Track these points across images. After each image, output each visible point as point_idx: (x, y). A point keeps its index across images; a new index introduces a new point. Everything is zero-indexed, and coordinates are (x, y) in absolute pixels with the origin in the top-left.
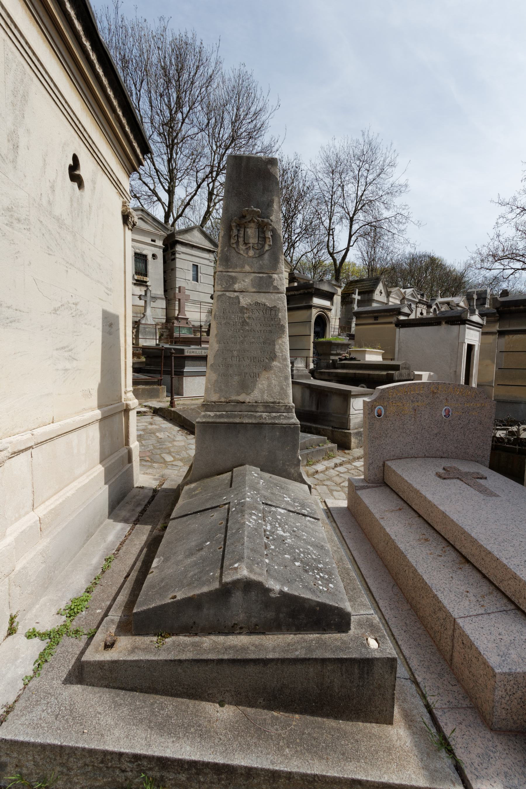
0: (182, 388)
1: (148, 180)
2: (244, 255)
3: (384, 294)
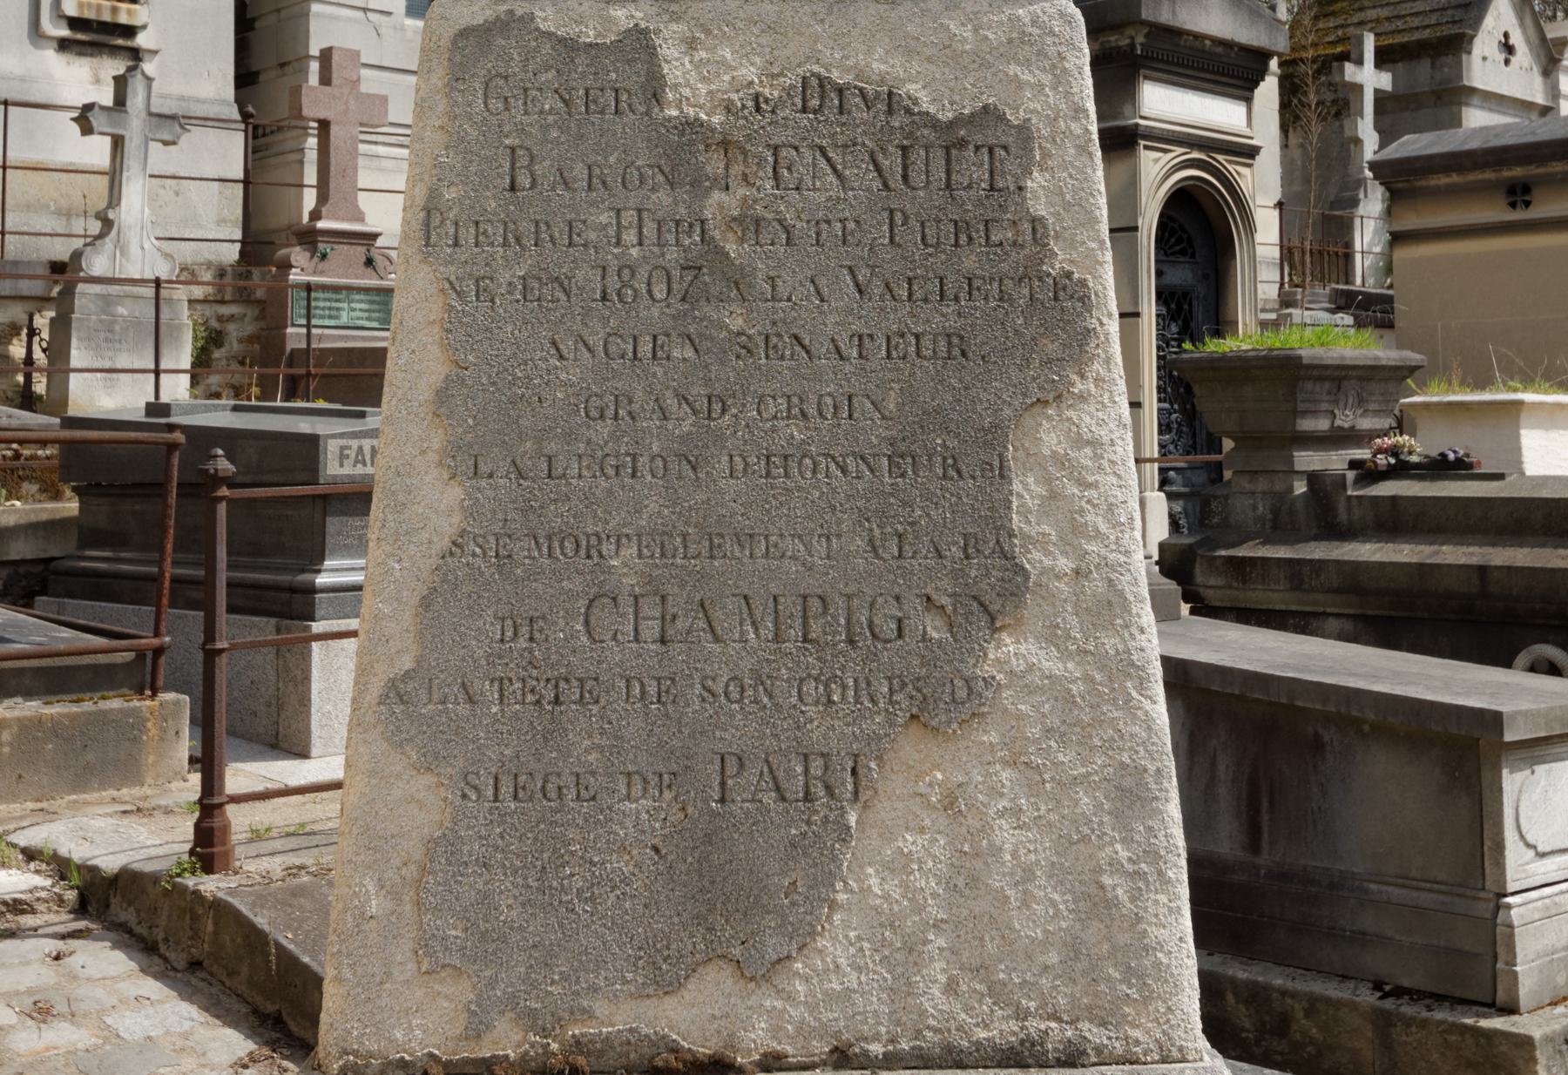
0: (305, 701)
3: (1523, 56)
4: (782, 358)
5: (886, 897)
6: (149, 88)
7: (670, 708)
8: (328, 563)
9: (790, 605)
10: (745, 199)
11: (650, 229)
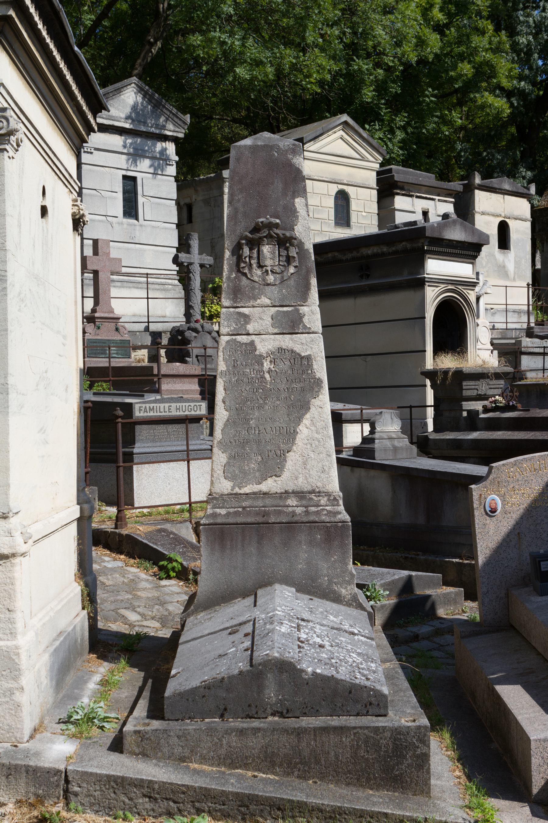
8: (136, 445)
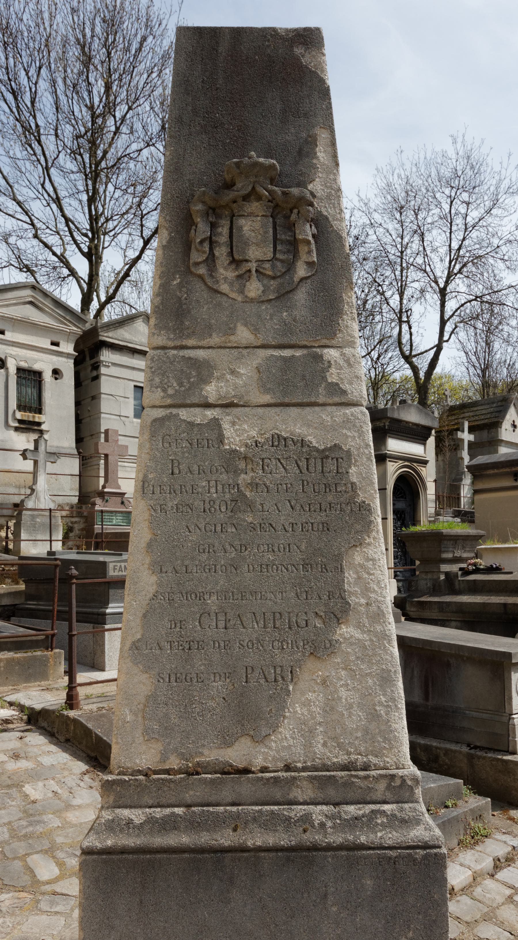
0: (103, 652)
1: (53, 240)
2: (233, 295)
4: (266, 531)
5: (303, 714)
6: (46, 443)
7: (228, 651)
8: (110, 605)
9: (269, 616)
10: (252, 477)
11: (220, 487)
